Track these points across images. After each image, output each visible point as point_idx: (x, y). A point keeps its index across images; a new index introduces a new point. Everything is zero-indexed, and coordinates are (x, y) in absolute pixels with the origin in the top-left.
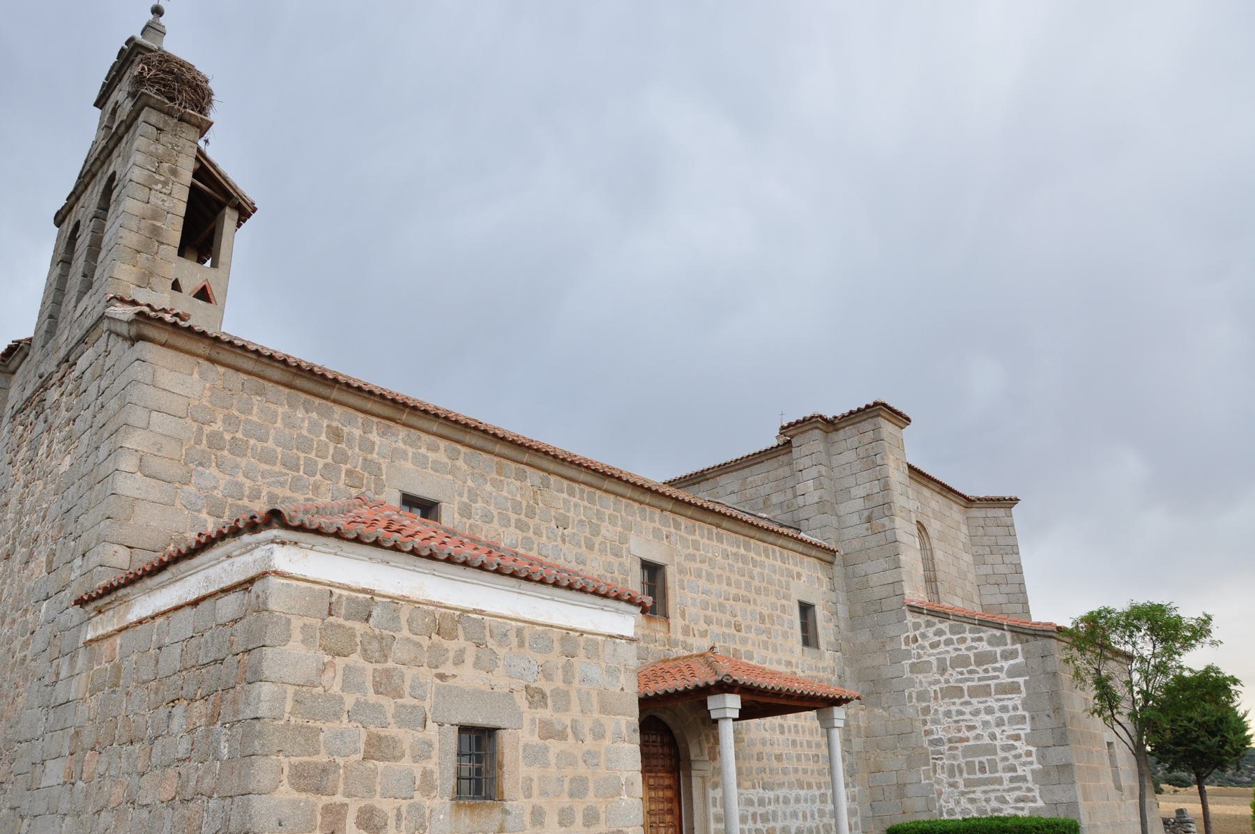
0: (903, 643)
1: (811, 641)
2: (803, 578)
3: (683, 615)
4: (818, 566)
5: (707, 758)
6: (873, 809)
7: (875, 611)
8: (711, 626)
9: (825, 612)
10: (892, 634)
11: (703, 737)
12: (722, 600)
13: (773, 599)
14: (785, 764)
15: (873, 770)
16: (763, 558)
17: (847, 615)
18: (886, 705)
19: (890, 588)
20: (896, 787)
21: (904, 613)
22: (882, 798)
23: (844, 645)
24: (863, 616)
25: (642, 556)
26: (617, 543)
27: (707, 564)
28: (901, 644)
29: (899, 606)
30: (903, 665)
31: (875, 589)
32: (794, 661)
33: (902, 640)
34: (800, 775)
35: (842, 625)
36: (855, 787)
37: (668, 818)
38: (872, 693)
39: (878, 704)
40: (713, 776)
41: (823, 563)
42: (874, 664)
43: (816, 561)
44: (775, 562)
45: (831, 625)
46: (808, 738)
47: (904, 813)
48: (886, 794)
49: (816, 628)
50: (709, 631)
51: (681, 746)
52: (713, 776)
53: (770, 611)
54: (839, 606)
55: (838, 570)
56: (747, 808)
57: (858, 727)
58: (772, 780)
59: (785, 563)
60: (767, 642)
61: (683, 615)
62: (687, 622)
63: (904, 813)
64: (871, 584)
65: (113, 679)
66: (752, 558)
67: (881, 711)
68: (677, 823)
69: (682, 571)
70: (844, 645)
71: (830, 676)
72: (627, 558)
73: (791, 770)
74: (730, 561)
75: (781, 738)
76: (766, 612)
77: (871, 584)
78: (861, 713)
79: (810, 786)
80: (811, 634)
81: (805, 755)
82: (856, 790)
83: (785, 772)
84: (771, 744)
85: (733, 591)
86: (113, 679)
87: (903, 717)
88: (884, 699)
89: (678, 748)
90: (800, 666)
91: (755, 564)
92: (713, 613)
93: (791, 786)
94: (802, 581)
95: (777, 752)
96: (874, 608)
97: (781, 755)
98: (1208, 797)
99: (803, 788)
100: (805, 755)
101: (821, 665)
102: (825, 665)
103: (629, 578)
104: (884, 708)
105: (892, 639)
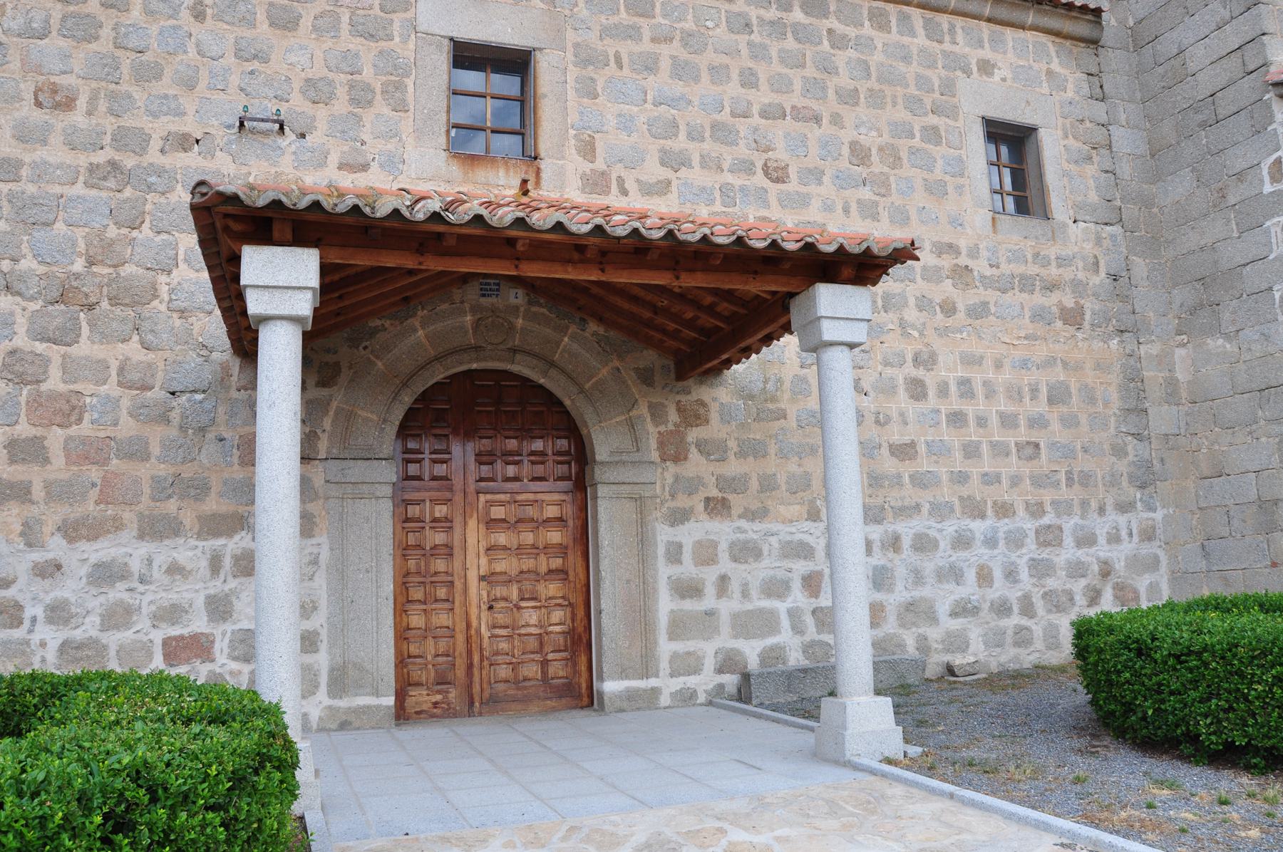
0: (1267, 179)
1: (1034, 202)
2: (998, 75)
3: (588, 150)
4: (1052, 49)
5: (655, 456)
6: (1206, 555)
7: (1204, 125)
8: (684, 172)
9: (1071, 142)
10: (1240, 165)
11: (643, 410)
12: (725, 116)
13: (902, 114)
14: (924, 464)
15: (1206, 472)
16: (867, 30)
17: (1143, 149)
18: (1232, 329)
19: (1234, 62)
20: (1255, 508)
21: (1269, 107)
22: (1225, 531)
23: (1130, 211)
24: (1178, 143)
25: (455, 34)
26: (377, 11)
27: (676, 43)
28: (1262, 181)
29: (1255, 97)
30: (1268, 231)
31: (1200, 76)
32: (963, 244)
33: (1265, 172)
34: (975, 488)
35: (1125, 170)
36: (1152, 509)
37: (552, 589)
38: (1202, 306)
39: (1215, 329)
40: (673, 496)
41: (1068, 43)
42: (1202, 243)
43: (1043, 38)
44: (906, 40)
45: (1091, 170)
46: (1003, 405)
47: (1274, 565)
48: (1235, 523)
49: (1041, 176)
50: (674, 183)
51: (584, 432)
52: (673, 496)
53: (886, 138)
54: (1116, 132)
55: (1115, 60)
56: (787, 564)
57: (1172, 383)
58: (880, 501)
59: (940, 42)
60: (876, 204)
61: (588, 150)
62: (600, 165)
63: (1274, 565)
64: (1192, 66)
65: (151, 402)
66: (830, 31)
67: (1220, 341)
68: (578, 599)
69: (587, 59)
70: (1130, 211)
71: (1081, 275)
72: (405, 41)
73: (945, 478)
74: (755, 37)
75: (913, 409)
76: (870, 139)
77: (1192, 66)
78: (1180, 353)
79: (1004, 510)
80: (1032, 193)
81: (993, 445)
82: (1159, 515)
83: (919, 481)
84: (877, 422)
85: (763, 96)
86: (151, 402)
87: (1271, 349)
88: (1226, 316)
89: (581, 436)
90: (984, 253)
91: (839, 42)
92: (692, 146)
93: (940, 511)
94: (997, 78)
95: (897, 439)
96: (1200, 117)
97: (912, 445)
98: (602, 491)
99: (983, 516)
100: (993, 445)
101: (1052, 251)
102: (1067, 252)
103: (409, 82)
104: (1227, 337)
105: (1240, 176)
